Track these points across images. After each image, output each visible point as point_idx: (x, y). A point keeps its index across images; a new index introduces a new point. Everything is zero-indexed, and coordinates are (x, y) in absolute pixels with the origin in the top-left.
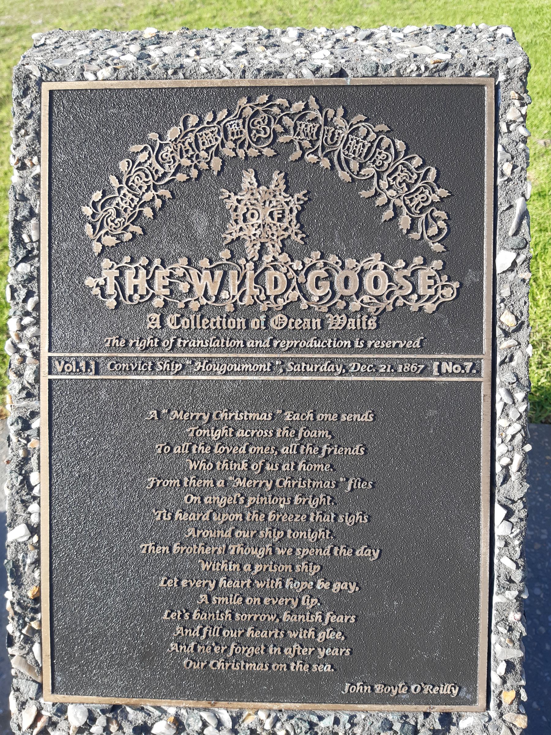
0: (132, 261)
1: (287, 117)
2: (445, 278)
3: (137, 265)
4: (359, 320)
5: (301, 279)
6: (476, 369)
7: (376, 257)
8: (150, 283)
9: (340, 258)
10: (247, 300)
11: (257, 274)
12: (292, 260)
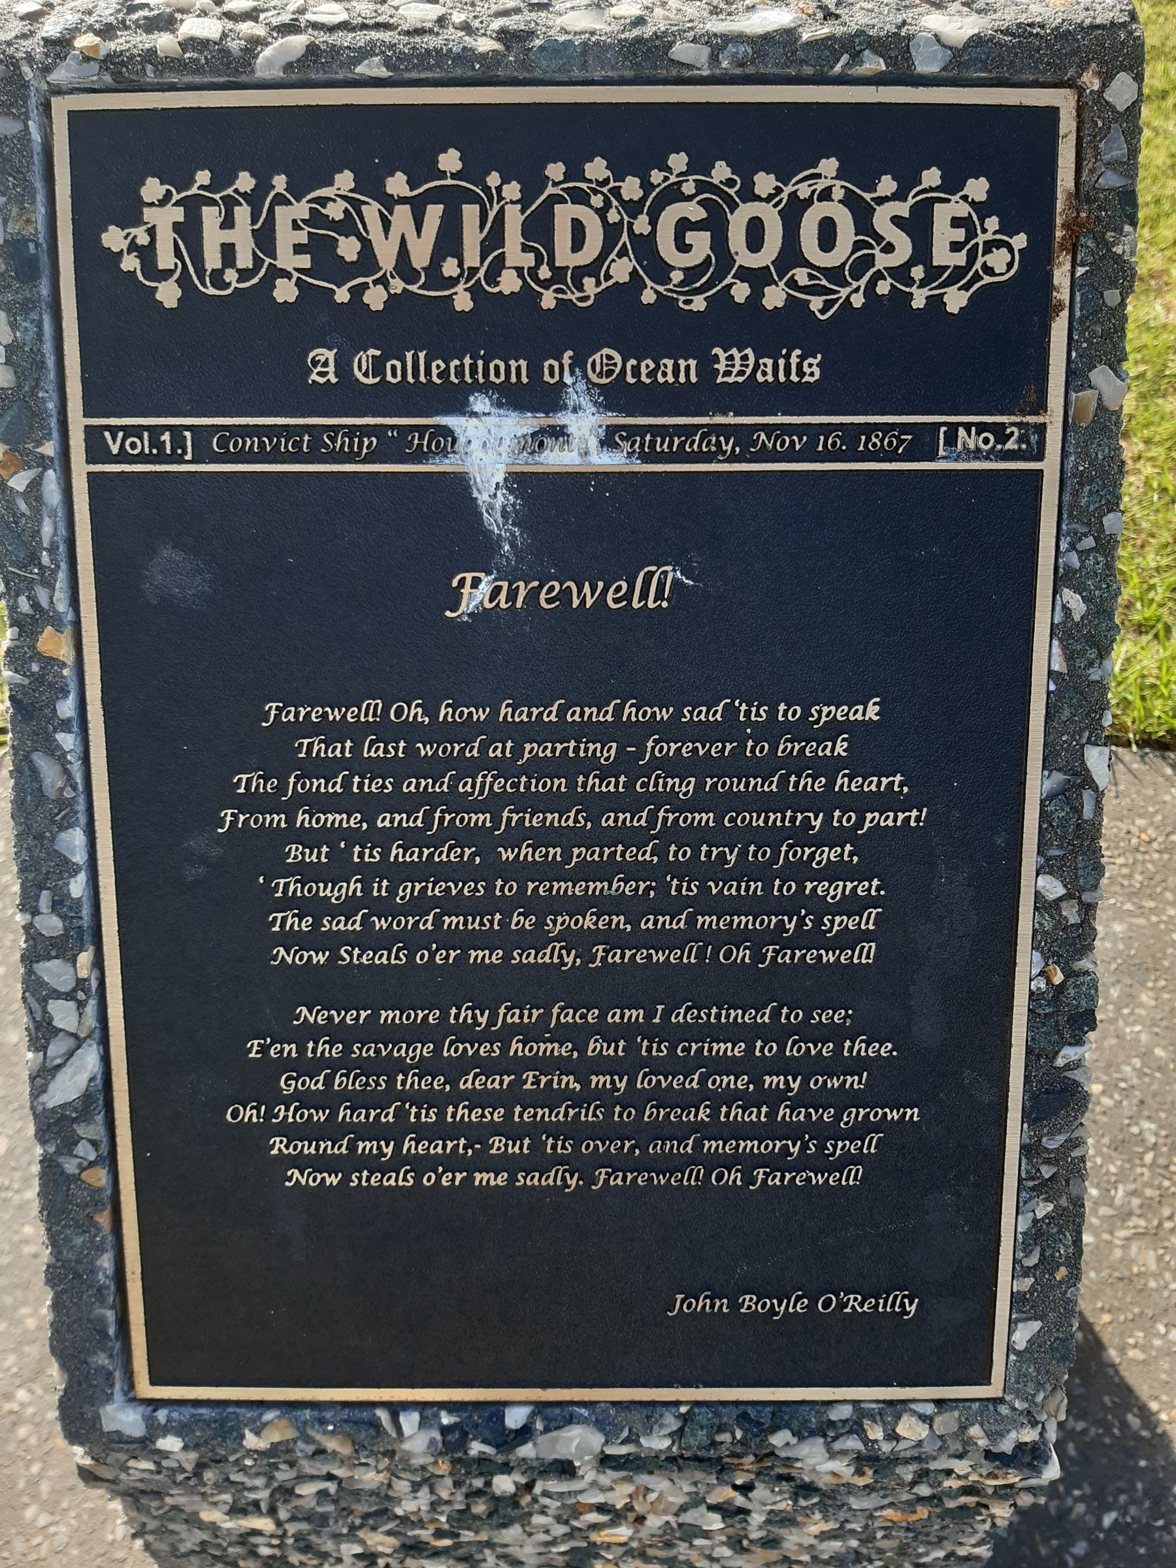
2: (993, 223)
5: (642, 225)
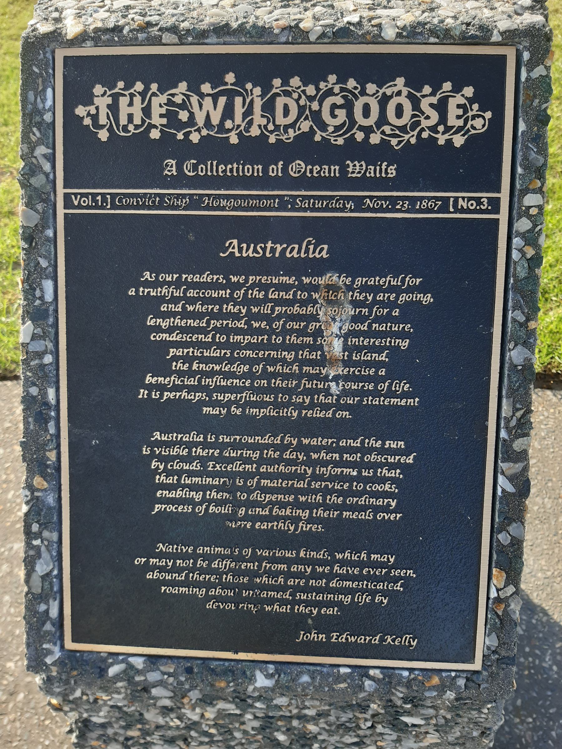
1: (313, 95)
2: (476, 106)
5: (315, 106)
6: (495, 204)
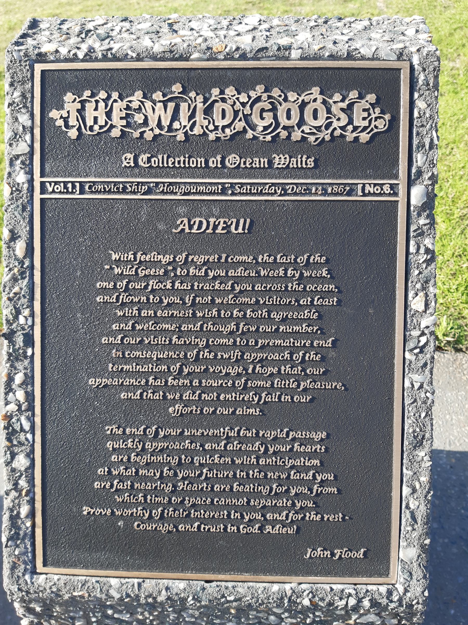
0: (93, 95)
2: (378, 110)
3: (97, 98)
4: (299, 160)
7: (316, 90)
8: (109, 114)
9: (282, 92)
10: (197, 131)
11: (206, 106)
12: (239, 94)
